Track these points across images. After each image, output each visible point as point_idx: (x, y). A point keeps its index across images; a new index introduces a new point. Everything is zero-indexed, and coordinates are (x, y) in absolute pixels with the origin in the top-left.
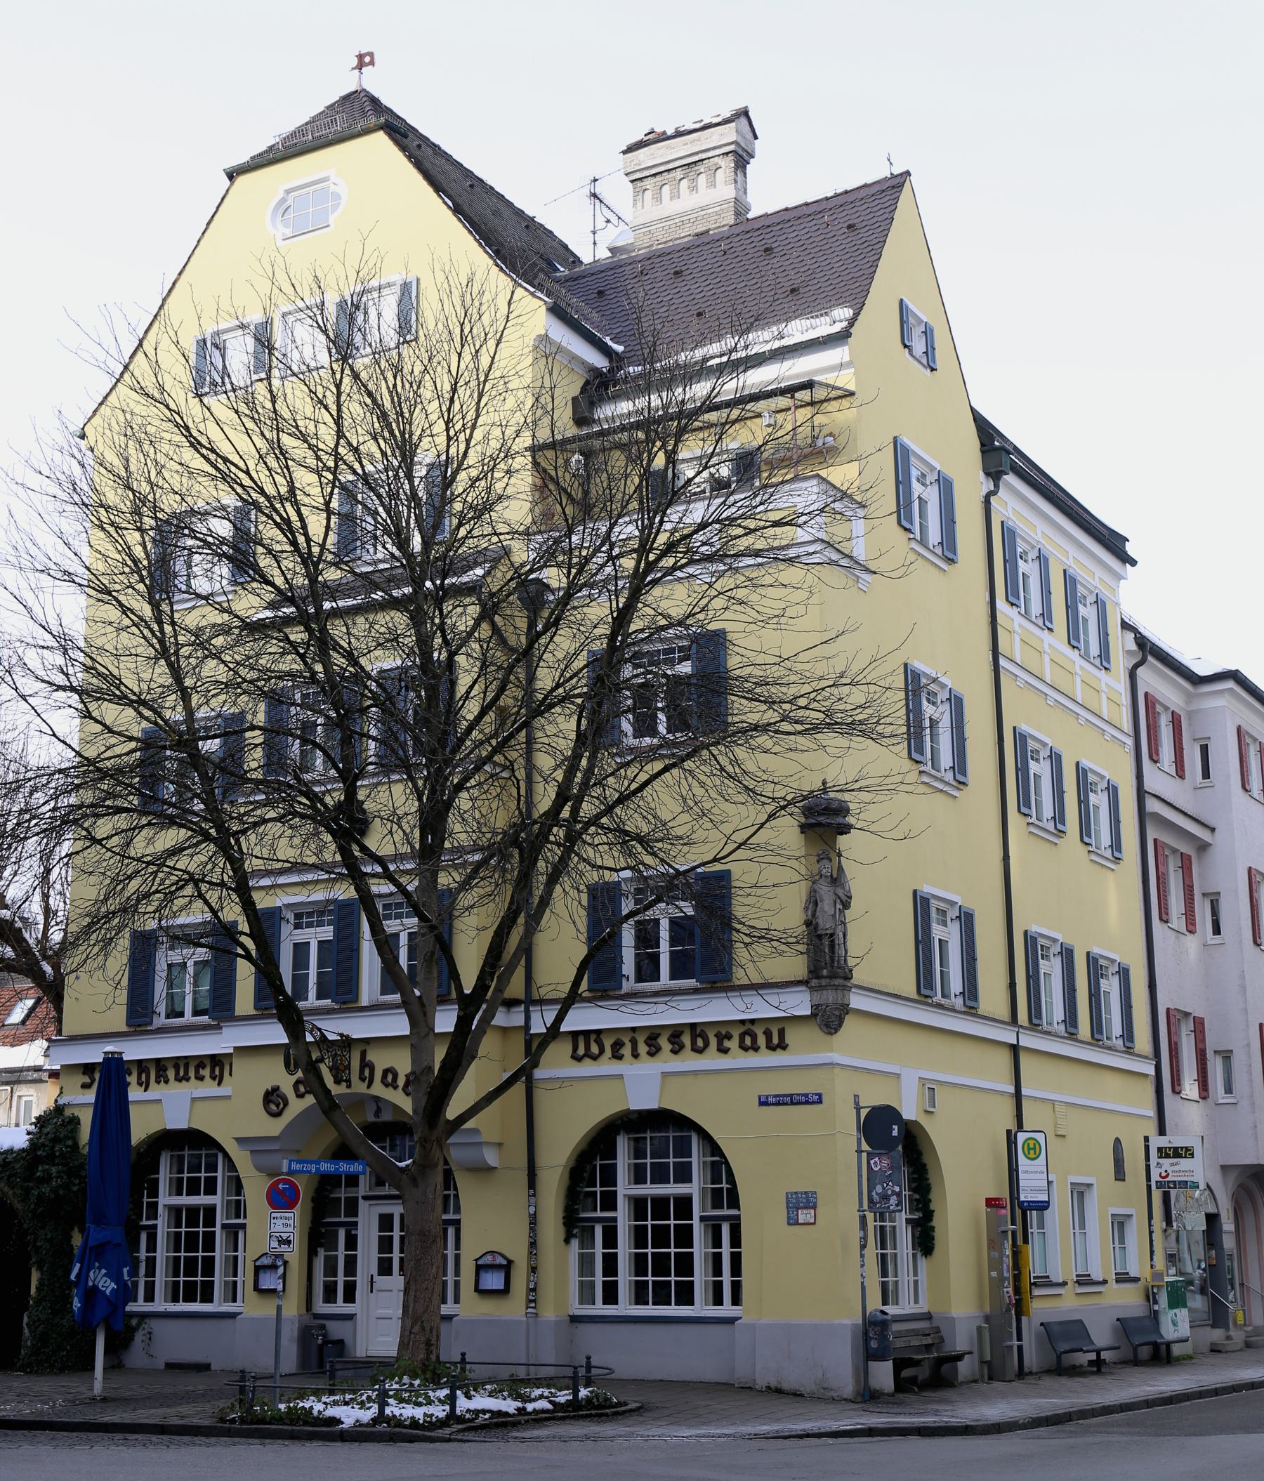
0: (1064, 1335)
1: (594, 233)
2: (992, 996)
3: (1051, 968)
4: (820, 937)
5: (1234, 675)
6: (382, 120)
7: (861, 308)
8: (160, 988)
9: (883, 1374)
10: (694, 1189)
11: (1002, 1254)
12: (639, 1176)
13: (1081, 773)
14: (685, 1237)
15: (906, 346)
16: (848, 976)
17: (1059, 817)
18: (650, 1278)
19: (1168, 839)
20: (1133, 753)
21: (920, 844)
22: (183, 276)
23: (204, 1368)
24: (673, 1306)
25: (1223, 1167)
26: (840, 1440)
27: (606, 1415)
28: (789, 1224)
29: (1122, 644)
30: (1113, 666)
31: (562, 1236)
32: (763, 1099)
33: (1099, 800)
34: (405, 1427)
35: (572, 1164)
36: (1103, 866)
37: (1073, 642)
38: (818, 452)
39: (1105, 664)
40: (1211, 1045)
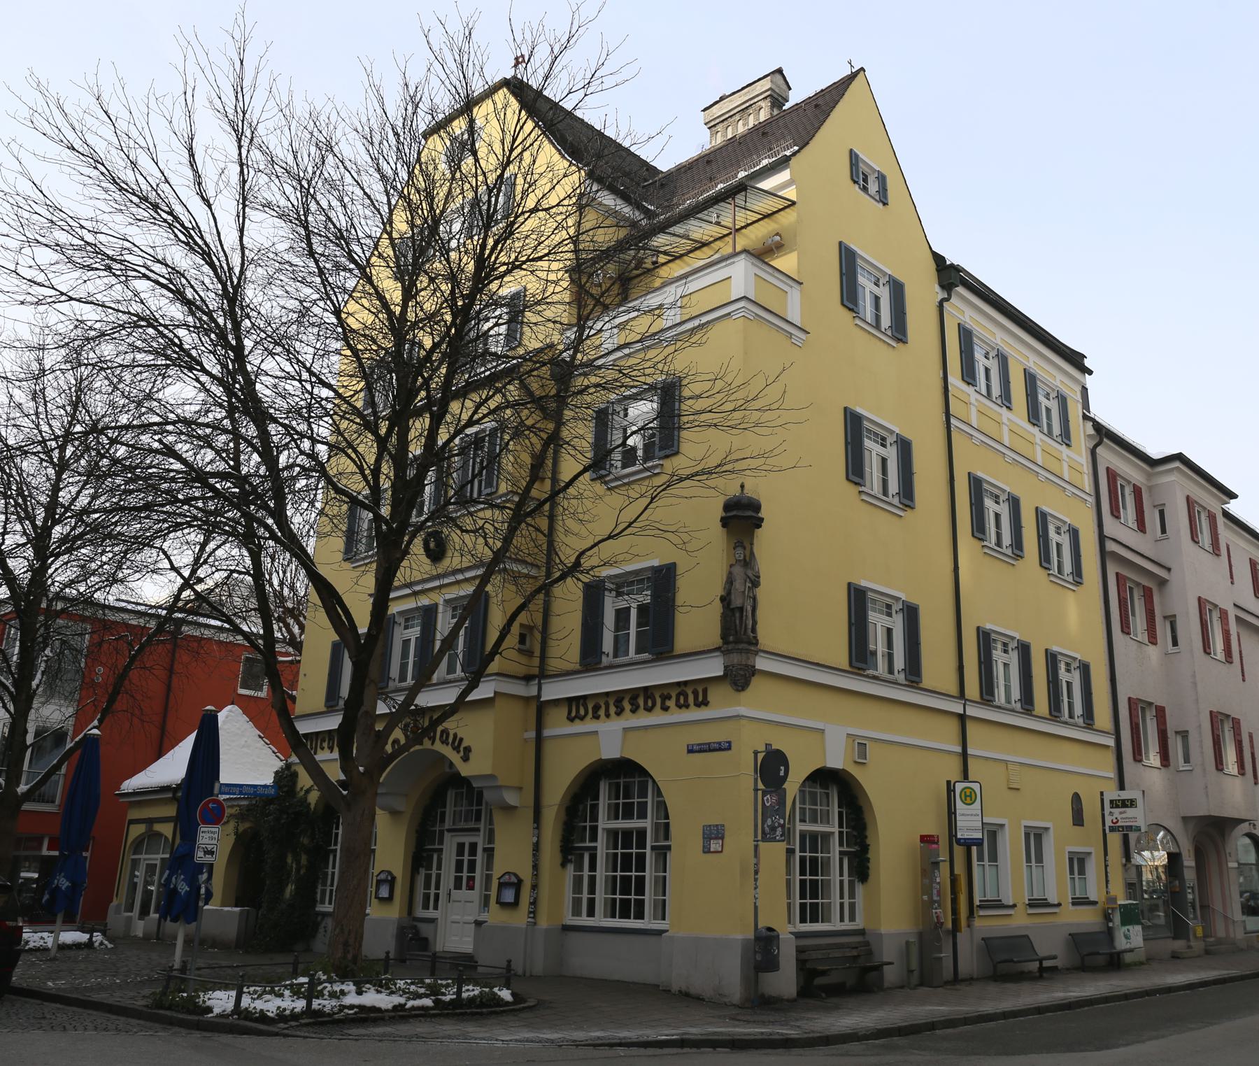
5: (1180, 457)
13: (1042, 518)
16: (755, 642)
20: (1095, 509)
27: (481, 1014)
40: (1171, 726)
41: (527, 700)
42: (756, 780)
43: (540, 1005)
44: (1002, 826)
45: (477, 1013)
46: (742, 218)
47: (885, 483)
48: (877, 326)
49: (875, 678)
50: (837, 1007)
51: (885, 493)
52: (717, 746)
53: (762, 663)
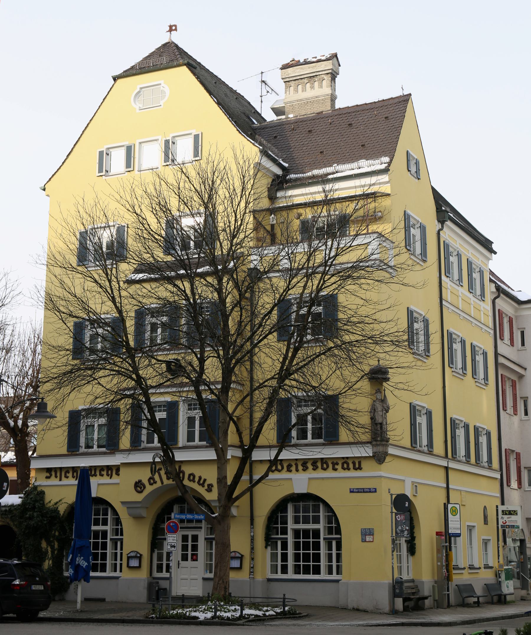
0: (466, 590)
1: (261, 96)
2: (438, 447)
3: (460, 433)
4: (376, 424)
6: (186, 62)
7: (393, 158)
8: (83, 435)
9: (399, 603)
10: (321, 526)
11: (442, 556)
12: (297, 521)
13: (473, 347)
14: (317, 546)
15: (409, 171)
16: (387, 440)
17: (464, 368)
18: (301, 563)
19: (507, 374)
21: (415, 383)
22: (92, 121)
23: (103, 600)
24: (302, 575)
25: (527, 519)
26: (392, 627)
27: (296, 617)
28: (362, 541)
29: (490, 288)
30: (486, 299)
31: (264, 545)
32: (352, 490)
33: (480, 358)
34: (225, 620)
35: (269, 515)
36: (481, 387)
37: (471, 290)
38: (375, 218)
39: (483, 298)
40: (523, 464)
42: (392, 508)
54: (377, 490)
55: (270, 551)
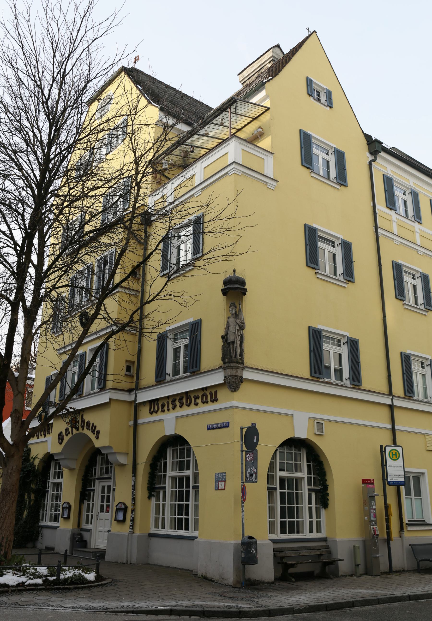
16: (243, 363)
24: (183, 531)
27: (69, 589)
35: (150, 462)
41: (130, 402)
42: (242, 445)
43: (113, 582)
44: (423, 474)
45: (67, 588)
46: (241, 122)
47: (416, 298)
48: (329, 178)
49: (327, 383)
50: (297, 589)
51: (416, 303)
52: (222, 425)
53: (246, 375)
54: (230, 424)
55: (155, 503)
